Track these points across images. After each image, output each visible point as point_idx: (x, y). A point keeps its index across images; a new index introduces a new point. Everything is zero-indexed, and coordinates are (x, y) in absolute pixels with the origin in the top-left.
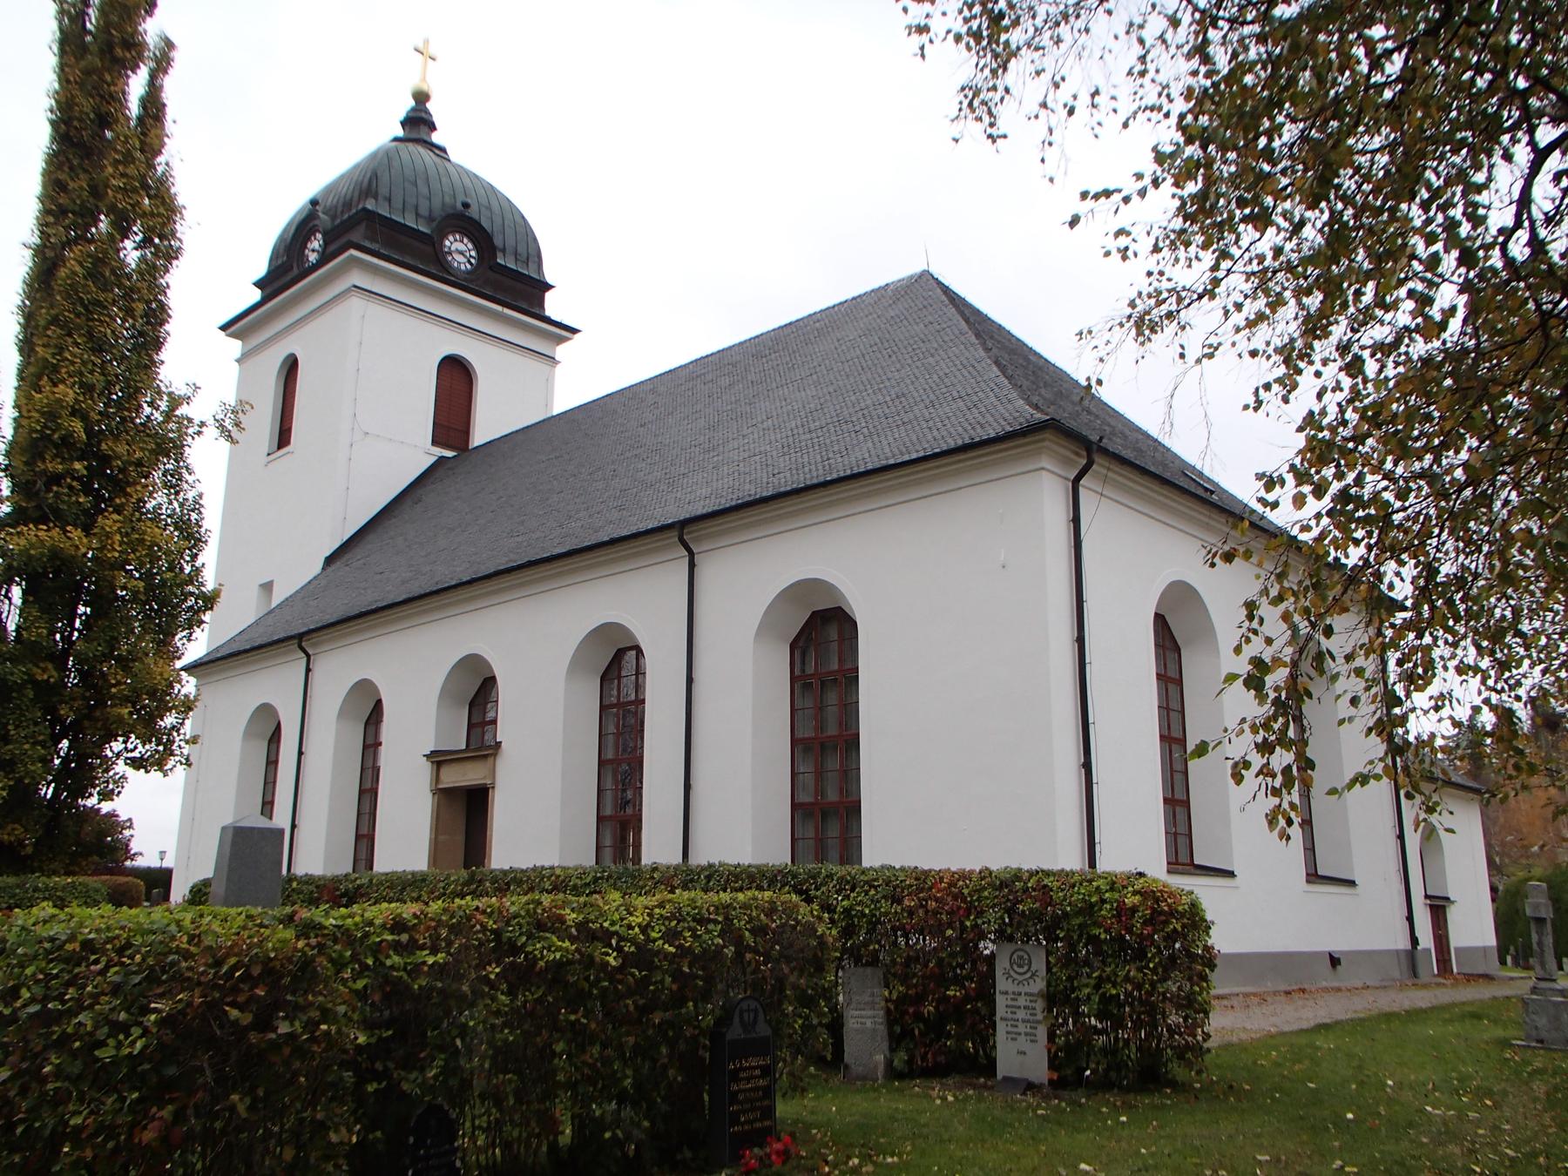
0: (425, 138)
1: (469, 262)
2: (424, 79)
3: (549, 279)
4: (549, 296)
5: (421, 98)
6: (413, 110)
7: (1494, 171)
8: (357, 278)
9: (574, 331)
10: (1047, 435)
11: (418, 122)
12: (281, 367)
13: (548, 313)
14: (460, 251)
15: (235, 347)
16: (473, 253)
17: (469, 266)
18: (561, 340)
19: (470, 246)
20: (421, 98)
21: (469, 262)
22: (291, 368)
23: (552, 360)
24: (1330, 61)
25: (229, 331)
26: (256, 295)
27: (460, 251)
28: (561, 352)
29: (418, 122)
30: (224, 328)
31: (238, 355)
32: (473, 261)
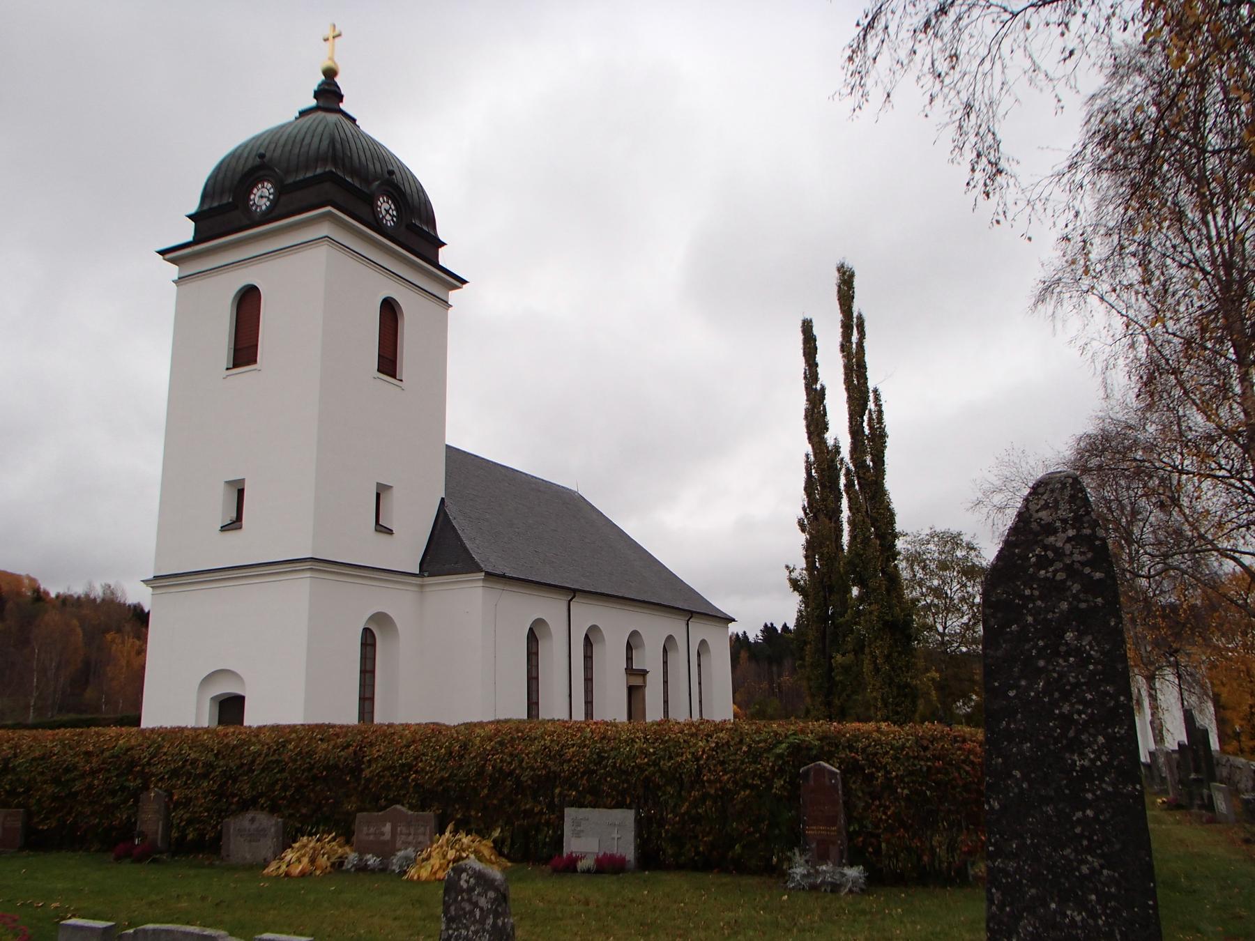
0: (336, 107)
1: (393, 220)
2: (331, 59)
3: (442, 237)
4: (442, 251)
5: (330, 74)
6: (323, 83)
7: (874, 55)
8: (324, 230)
9: (464, 282)
10: (234, 515)
11: (329, 94)
12: (233, 302)
13: (441, 263)
14: (385, 206)
15: (173, 271)
16: (395, 213)
17: (392, 224)
18: (455, 287)
19: (270, 186)
20: (330, 74)
21: (393, 220)
22: (248, 300)
23: (446, 304)
24: (744, 847)
25: (168, 256)
26: (187, 232)
27: (385, 206)
28: (454, 296)
29: (329, 94)
30: (162, 253)
31: (176, 278)
32: (395, 219)
